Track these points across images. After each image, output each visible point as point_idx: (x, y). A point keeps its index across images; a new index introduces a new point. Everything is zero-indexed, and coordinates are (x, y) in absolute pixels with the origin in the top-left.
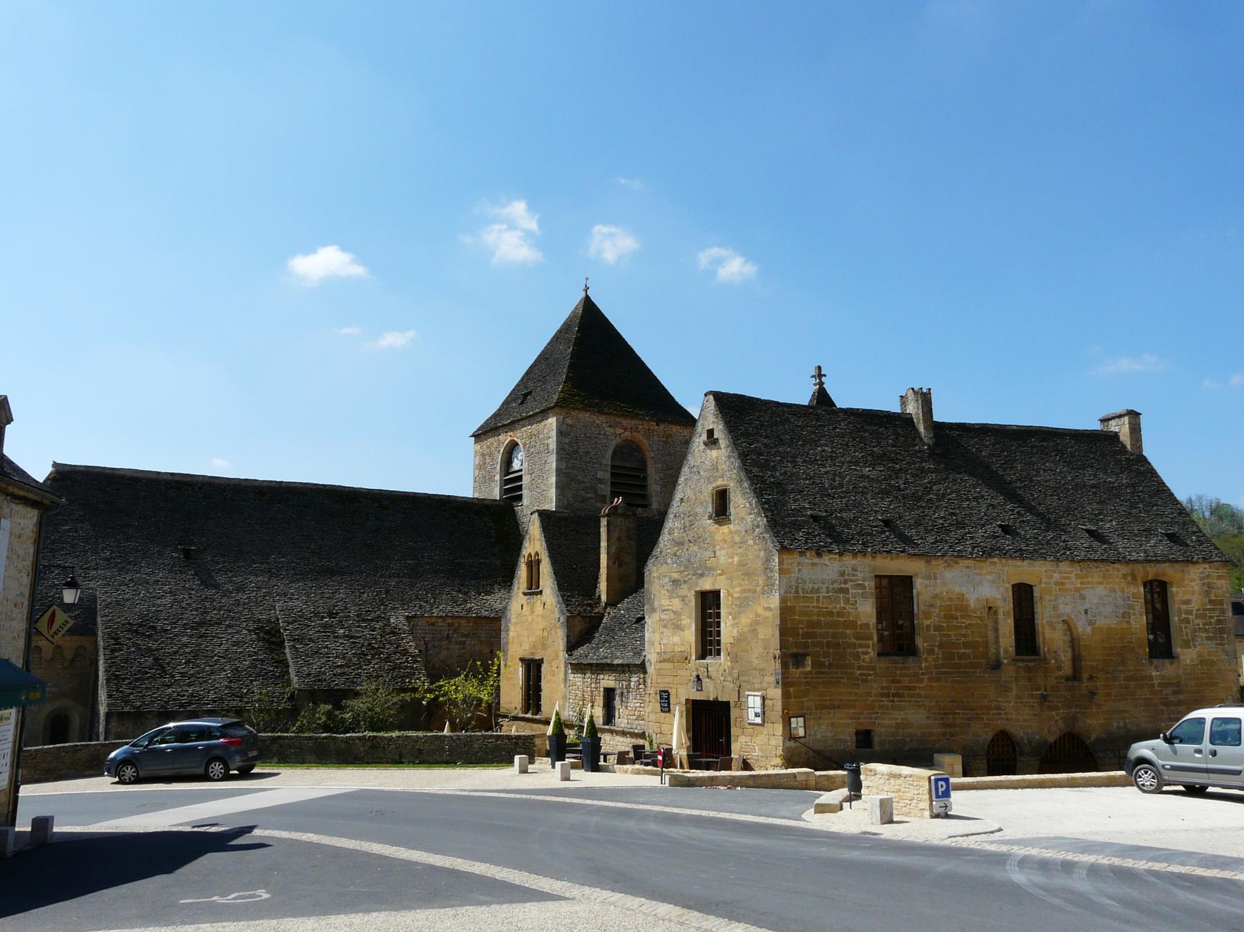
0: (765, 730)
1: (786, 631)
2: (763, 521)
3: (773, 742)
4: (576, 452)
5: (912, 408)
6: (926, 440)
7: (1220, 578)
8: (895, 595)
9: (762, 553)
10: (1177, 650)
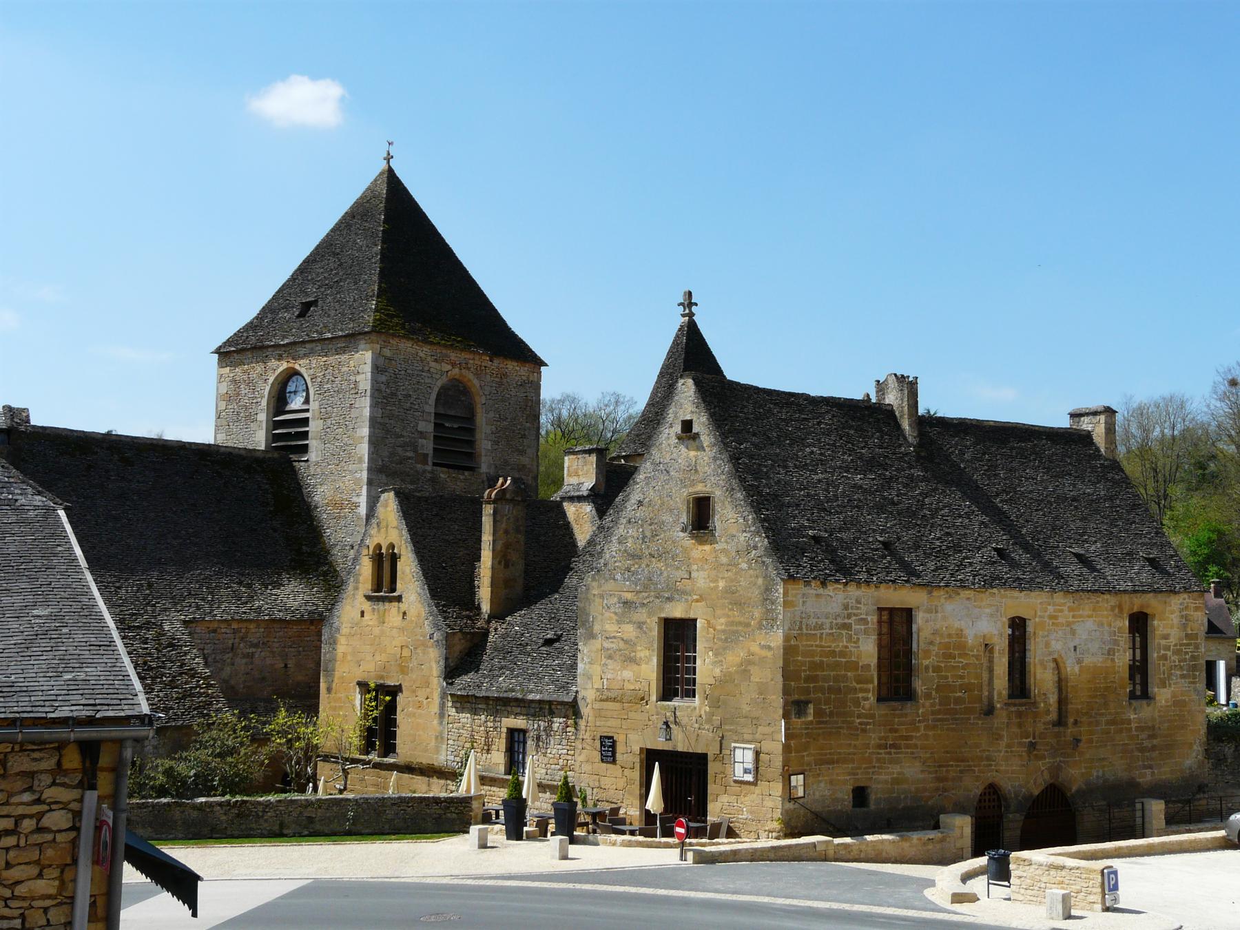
0: (757, 790)
1: (788, 674)
2: (762, 542)
3: (769, 803)
4: (393, 394)
5: (892, 398)
6: (910, 439)
7: (1197, 609)
8: (897, 628)
9: (760, 581)
10: (1154, 689)
